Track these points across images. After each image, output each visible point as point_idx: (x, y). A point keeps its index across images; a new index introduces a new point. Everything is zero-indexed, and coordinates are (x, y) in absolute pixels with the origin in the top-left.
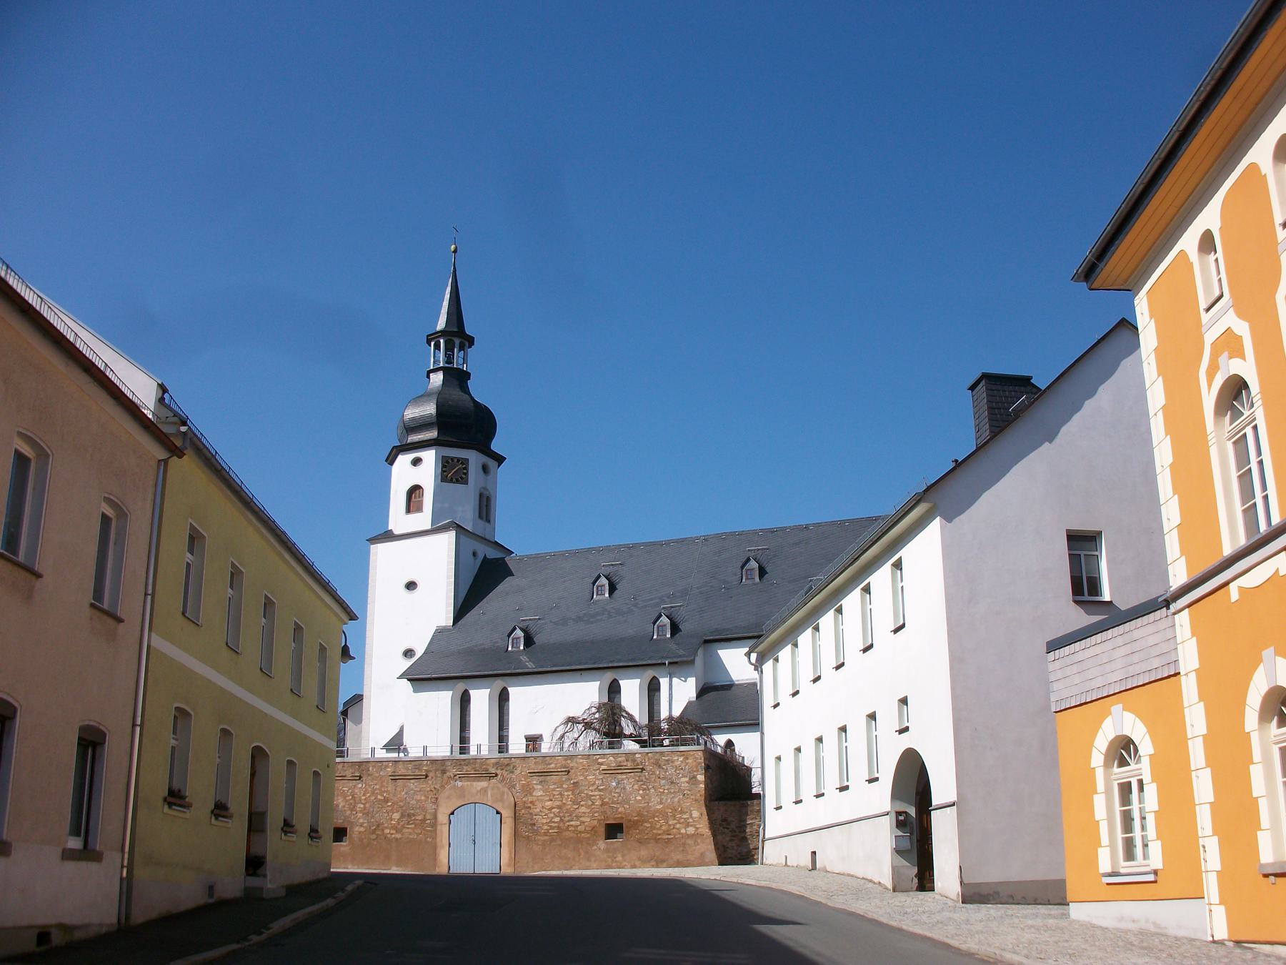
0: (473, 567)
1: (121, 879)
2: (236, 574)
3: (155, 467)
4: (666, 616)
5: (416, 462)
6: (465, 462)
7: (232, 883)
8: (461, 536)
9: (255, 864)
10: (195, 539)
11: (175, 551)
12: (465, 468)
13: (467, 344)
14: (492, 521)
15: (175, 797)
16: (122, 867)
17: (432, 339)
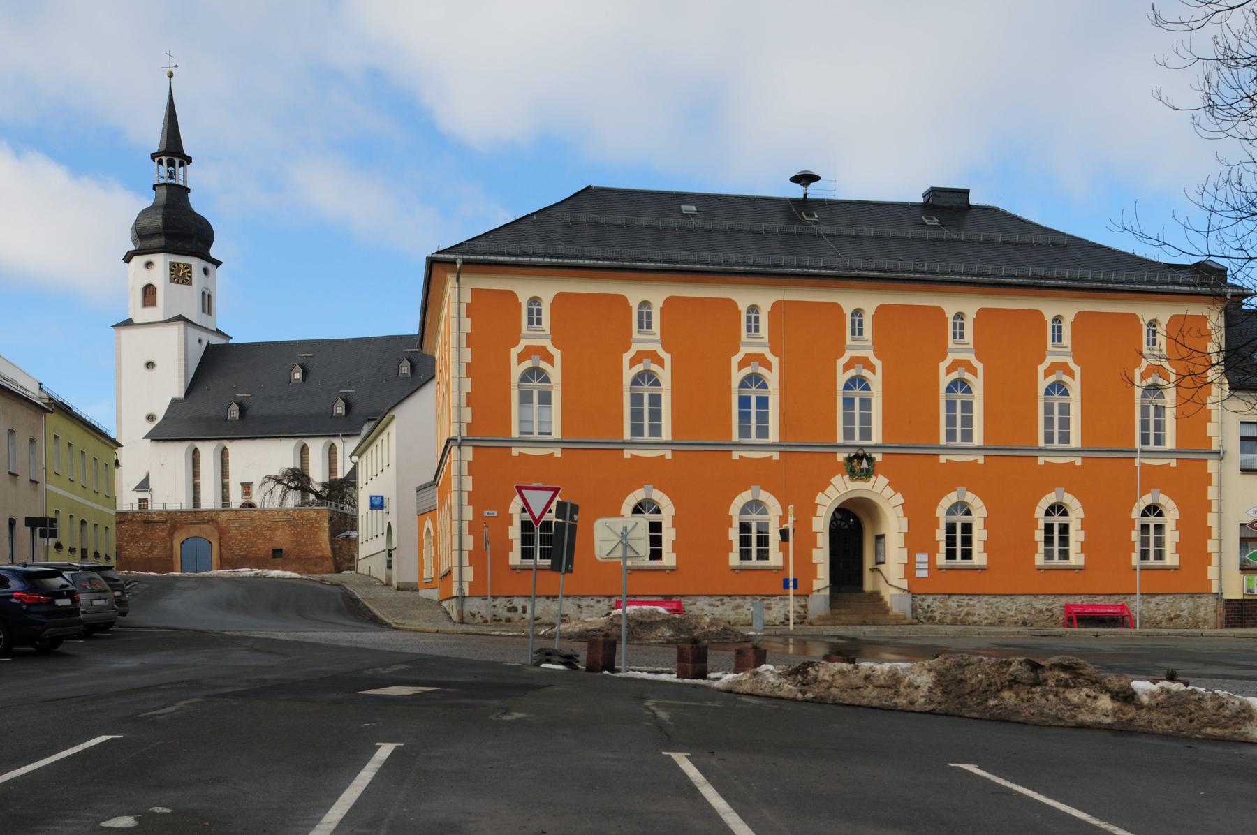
0: (198, 352)
4: (342, 400)
5: (148, 265)
6: (188, 267)
12: (189, 272)
13: (186, 162)
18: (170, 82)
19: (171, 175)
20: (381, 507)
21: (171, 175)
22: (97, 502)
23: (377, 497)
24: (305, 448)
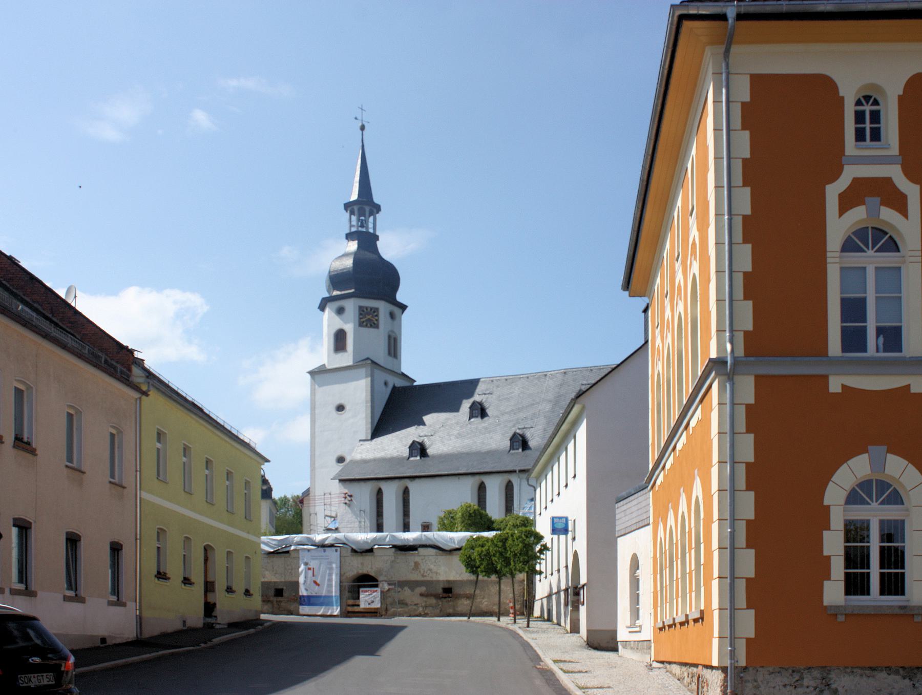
1: (137, 616)
2: (186, 450)
3: (134, 403)
6: (375, 311)
7: (196, 618)
8: (375, 370)
9: (209, 608)
10: (160, 436)
11: (150, 444)
14: (398, 357)
15: (161, 575)
16: (136, 610)
17: (349, 207)
18: (362, 135)
19: (363, 224)
20: (565, 531)
21: (363, 224)
22: (231, 524)
23: (560, 518)
24: (482, 485)
